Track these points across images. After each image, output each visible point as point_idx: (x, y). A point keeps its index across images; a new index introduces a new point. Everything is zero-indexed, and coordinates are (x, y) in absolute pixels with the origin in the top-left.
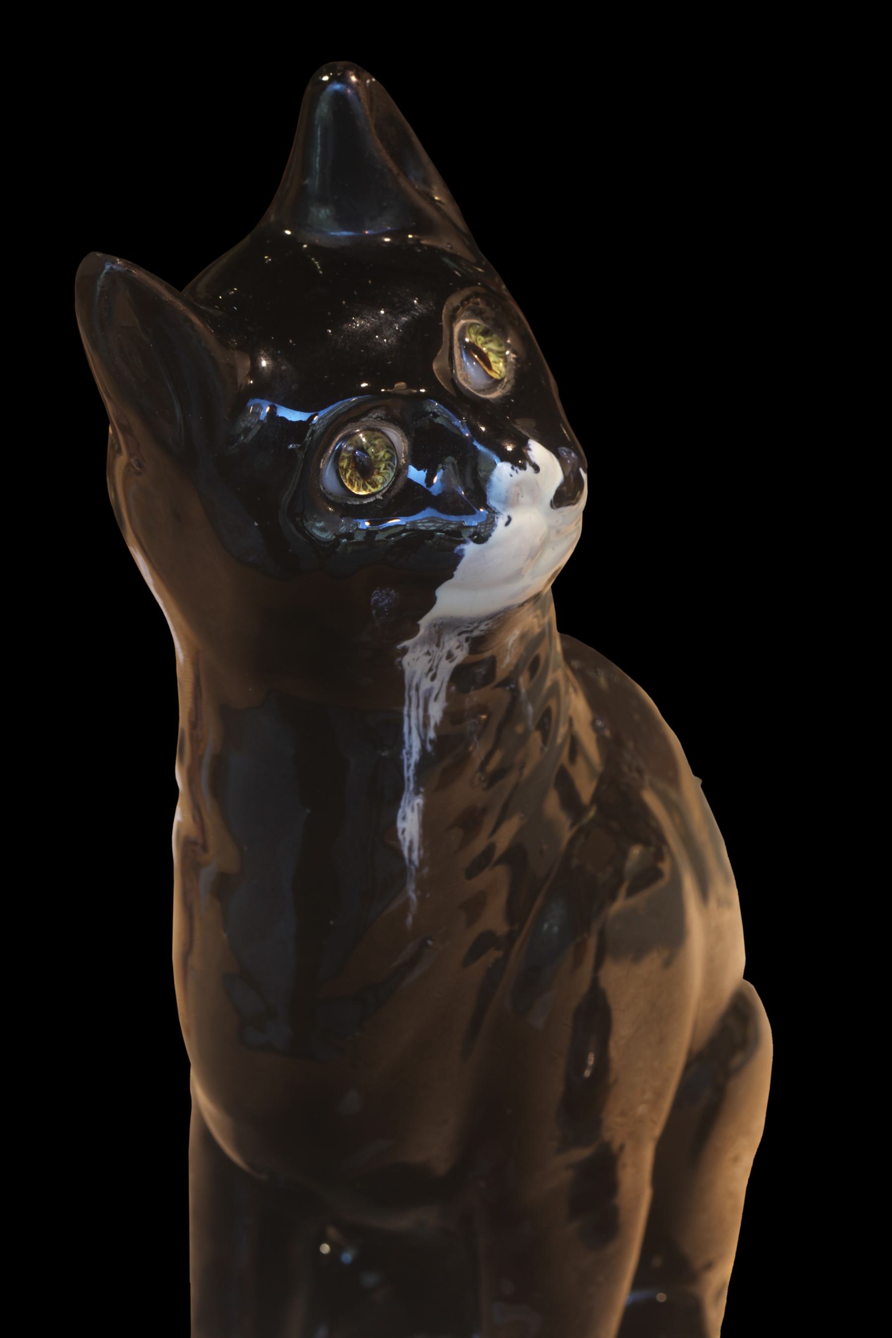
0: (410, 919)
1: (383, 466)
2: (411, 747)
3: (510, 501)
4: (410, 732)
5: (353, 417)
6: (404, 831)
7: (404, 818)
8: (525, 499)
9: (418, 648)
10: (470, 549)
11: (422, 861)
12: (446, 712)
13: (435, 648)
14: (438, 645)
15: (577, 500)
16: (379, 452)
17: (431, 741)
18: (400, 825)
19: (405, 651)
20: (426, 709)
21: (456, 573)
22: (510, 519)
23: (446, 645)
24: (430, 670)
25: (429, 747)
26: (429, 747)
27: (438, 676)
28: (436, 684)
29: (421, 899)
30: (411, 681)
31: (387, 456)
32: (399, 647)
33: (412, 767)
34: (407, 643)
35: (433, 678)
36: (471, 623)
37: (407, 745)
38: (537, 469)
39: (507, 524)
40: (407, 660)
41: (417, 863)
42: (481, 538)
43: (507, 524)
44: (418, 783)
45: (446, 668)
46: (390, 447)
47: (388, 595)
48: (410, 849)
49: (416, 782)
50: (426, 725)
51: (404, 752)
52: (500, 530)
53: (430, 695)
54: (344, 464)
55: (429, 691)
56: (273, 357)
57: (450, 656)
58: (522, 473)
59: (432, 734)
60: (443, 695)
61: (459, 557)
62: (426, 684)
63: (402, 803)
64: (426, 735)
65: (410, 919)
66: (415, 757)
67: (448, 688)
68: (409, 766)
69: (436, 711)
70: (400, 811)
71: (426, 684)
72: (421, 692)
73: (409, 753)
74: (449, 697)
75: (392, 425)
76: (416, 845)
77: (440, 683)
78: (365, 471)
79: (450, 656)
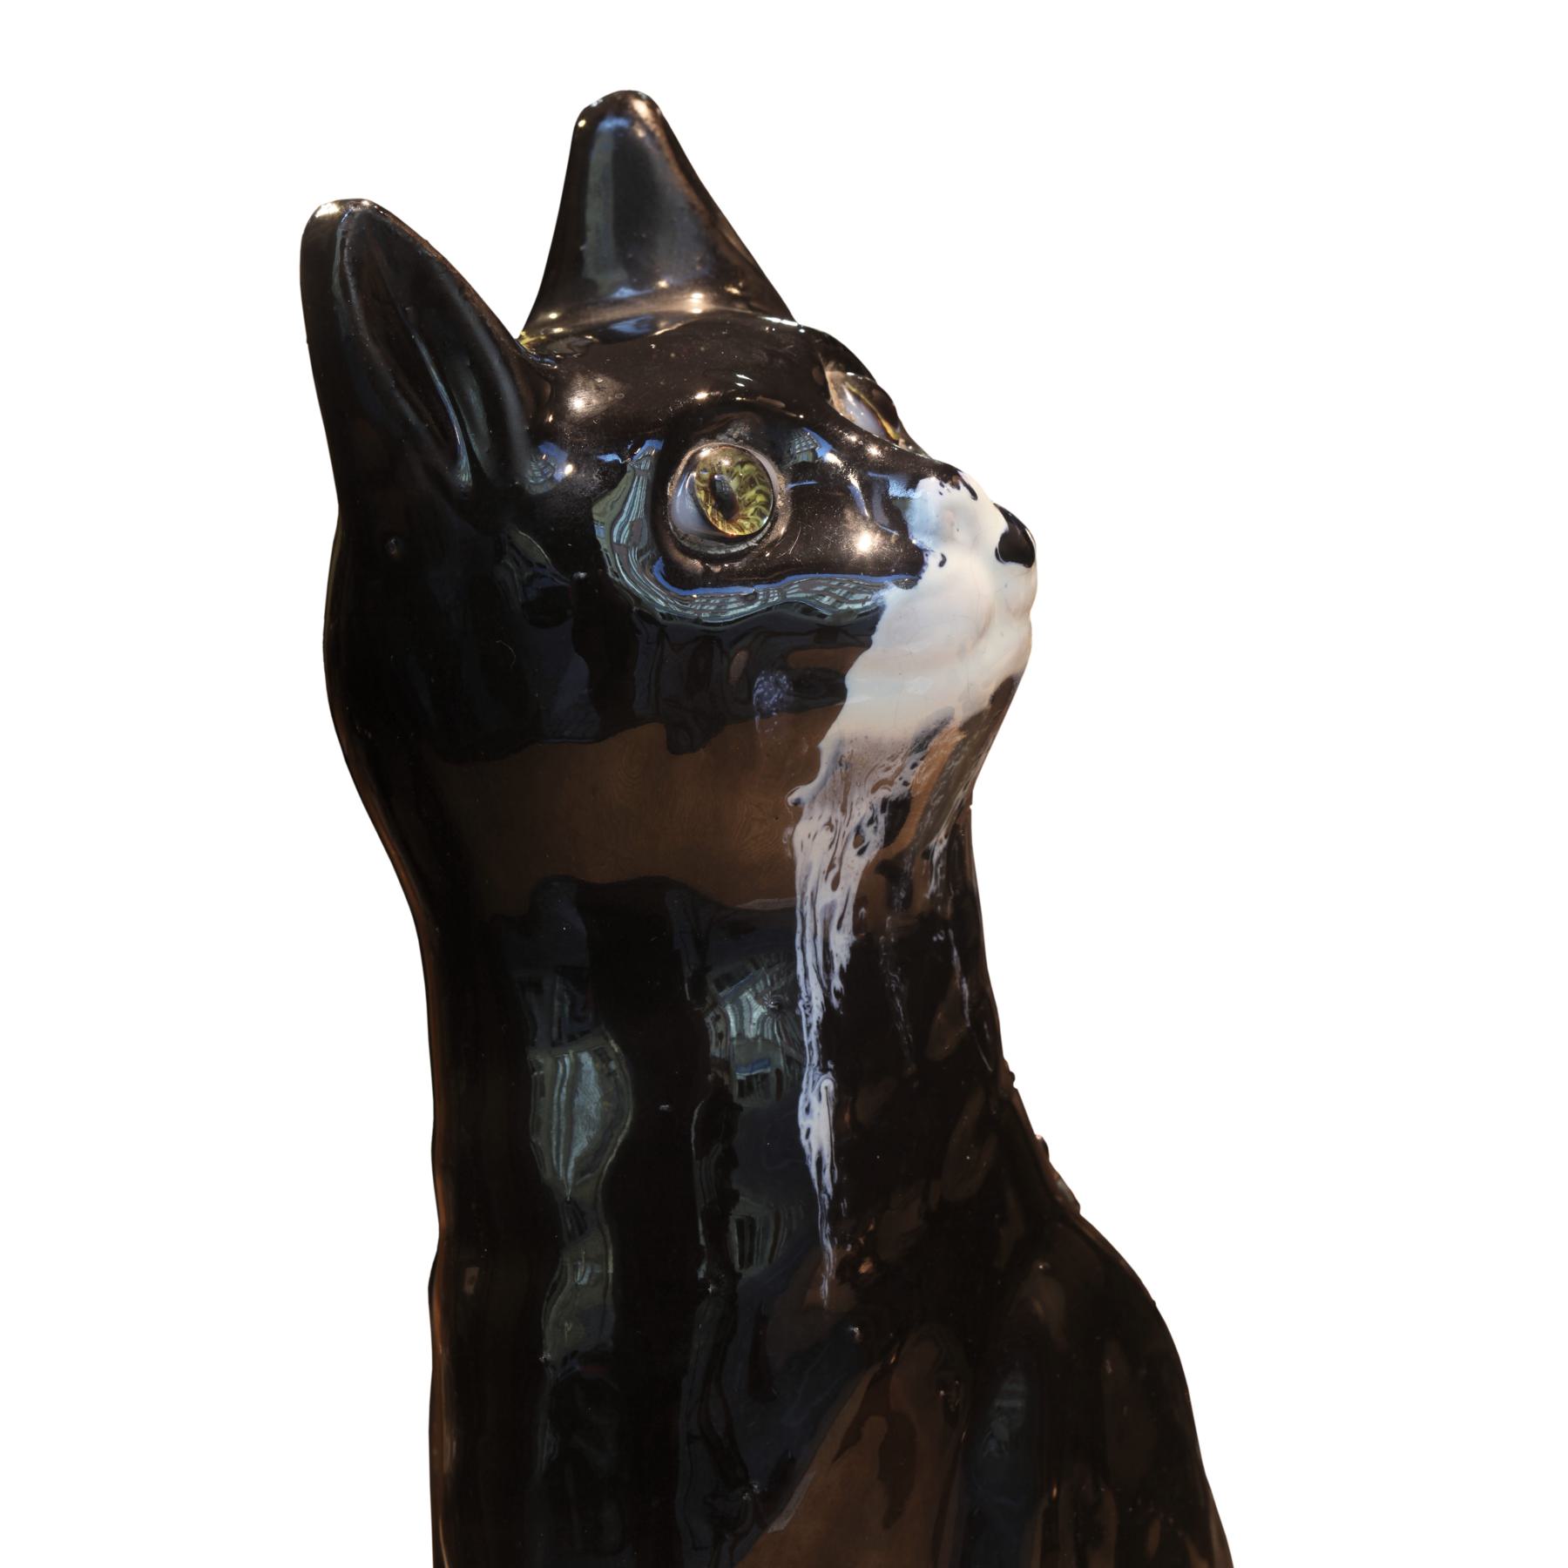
1: (752, 510)
2: (809, 998)
4: (806, 975)
6: (808, 1131)
7: (808, 1110)
8: (962, 535)
9: (817, 806)
10: (892, 595)
11: (837, 1187)
12: (854, 949)
13: (838, 815)
14: (844, 810)
17: (838, 994)
18: (803, 1122)
20: (826, 944)
23: (855, 812)
24: (831, 866)
25: (835, 1002)
26: (835, 1002)
27: (842, 883)
30: (805, 886)
31: (760, 498)
32: (791, 799)
33: (814, 1029)
34: (802, 792)
35: (835, 885)
36: (893, 758)
37: (804, 994)
39: (942, 564)
41: (830, 1190)
43: (942, 564)
44: (825, 1055)
45: (855, 866)
47: (777, 684)
48: (819, 1162)
49: (821, 1052)
50: (828, 967)
51: (800, 1004)
53: (831, 917)
55: (830, 908)
56: (546, 417)
59: (837, 983)
60: (848, 921)
62: (826, 896)
63: (804, 1085)
64: (829, 982)
66: (817, 1014)
67: (856, 908)
68: (809, 1028)
69: (841, 944)
70: (802, 1097)
71: (826, 896)
72: (819, 906)
73: (808, 1007)
74: (856, 929)
75: (547, 1175)
76: (827, 1161)
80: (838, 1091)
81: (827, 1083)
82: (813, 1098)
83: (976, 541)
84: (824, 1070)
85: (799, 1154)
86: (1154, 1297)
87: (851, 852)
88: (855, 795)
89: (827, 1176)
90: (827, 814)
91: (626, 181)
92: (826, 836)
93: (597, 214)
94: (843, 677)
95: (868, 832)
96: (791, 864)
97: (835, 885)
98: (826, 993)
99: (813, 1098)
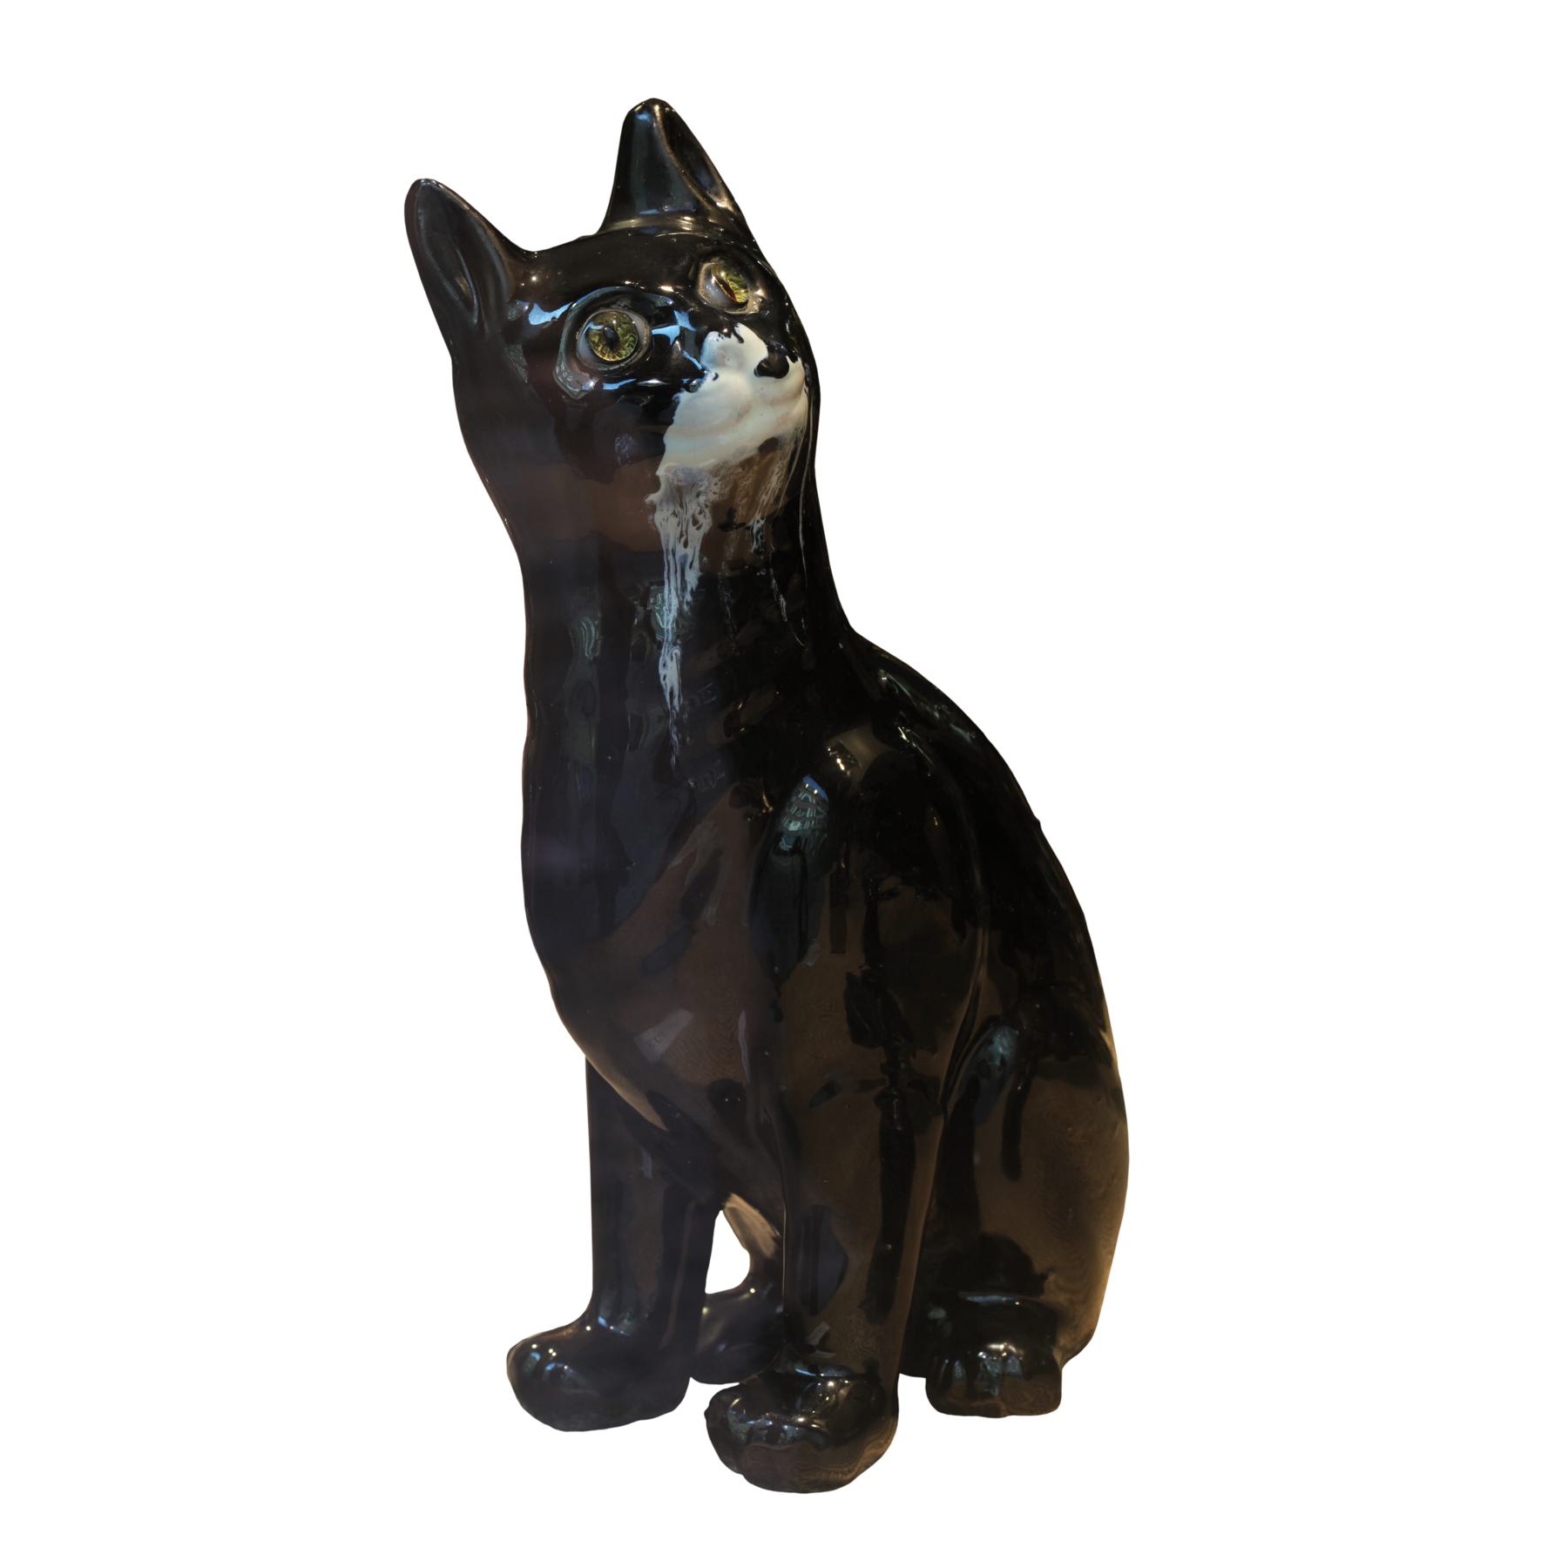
3: (719, 361)
10: (684, 396)
12: (700, 579)
15: (550, 310)
16: (694, 283)
18: (662, 672)
21: (675, 418)
22: (717, 377)
25: (686, 608)
28: (689, 551)
29: (682, 742)
34: (653, 497)
35: (686, 545)
38: (741, 340)
42: (688, 388)
45: (696, 536)
48: (671, 694)
50: (684, 588)
52: (708, 384)
55: (685, 557)
57: (695, 522)
59: (688, 598)
60: (696, 564)
62: (680, 550)
66: (674, 614)
67: (701, 559)
69: (692, 578)
76: (676, 692)
77: (692, 552)
78: (613, 343)
79: (695, 522)
80: (683, 656)
81: (677, 651)
82: (668, 659)
83: (741, 366)
84: (675, 644)
86: (1037, 812)
87: (692, 529)
88: (687, 499)
89: (676, 701)
91: (659, 152)
92: (674, 520)
93: (637, 178)
94: (662, 436)
95: (700, 518)
97: (686, 545)
98: (681, 604)
99: (668, 659)
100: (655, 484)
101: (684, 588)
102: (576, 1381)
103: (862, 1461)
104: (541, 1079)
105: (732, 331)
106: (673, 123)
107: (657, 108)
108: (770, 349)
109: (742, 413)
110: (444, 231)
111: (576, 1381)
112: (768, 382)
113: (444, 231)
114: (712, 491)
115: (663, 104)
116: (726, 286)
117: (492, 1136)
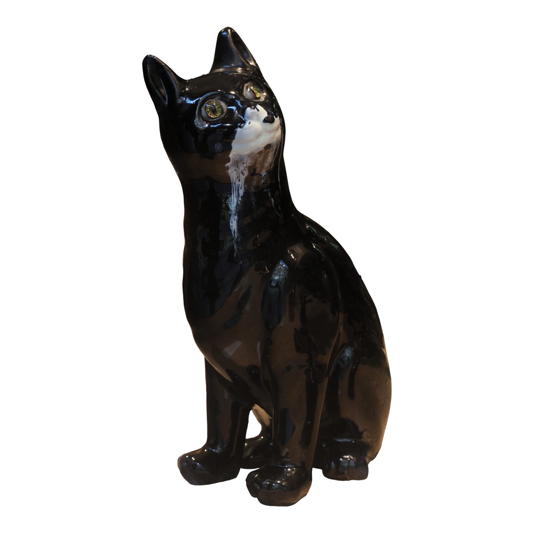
0: (235, 255)
5: (212, 97)
8: (255, 118)
9: (232, 167)
10: (239, 130)
11: (238, 237)
12: (244, 193)
18: (231, 224)
19: (228, 168)
25: (239, 202)
28: (240, 183)
29: (238, 249)
34: (228, 164)
35: (239, 181)
38: (258, 110)
40: (230, 171)
42: (240, 127)
45: (243, 178)
46: (221, 107)
48: (234, 232)
50: (239, 196)
52: (247, 125)
54: (208, 110)
55: (239, 185)
57: (242, 173)
58: (253, 110)
59: (240, 199)
60: (243, 187)
61: (235, 132)
62: (237, 183)
65: (235, 255)
69: (241, 192)
76: (236, 232)
77: (241, 183)
78: (214, 111)
79: (242, 173)
81: (236, 217)
83: (258, 119)
85: (230, 230)
87: (241, 175)
89: (236, 234)
90: (234, 168)
91: (229, 46)
92: (235, 172)
95: (244, 172)
96: (229, 177)
97: (239, 181)
100: (228, 160)
101: (239, 196)
102: (201, 468)
103: (300, 496)
104: (190, 365)
105: (255, 107)
106: (235, 35)
107: (229, 30)
108: (268, 113)
109: (259, 135)
110: (155, 73)
111: (201, 468)
112: (268, 125)
113: (155, 73)
114: (248, 162)
115: (231, 29)
116: (253, 92)
117: (172, 385)
